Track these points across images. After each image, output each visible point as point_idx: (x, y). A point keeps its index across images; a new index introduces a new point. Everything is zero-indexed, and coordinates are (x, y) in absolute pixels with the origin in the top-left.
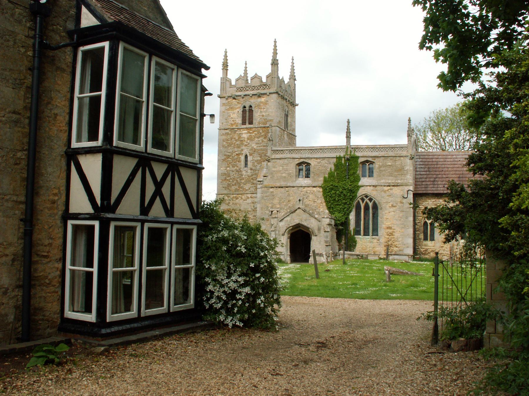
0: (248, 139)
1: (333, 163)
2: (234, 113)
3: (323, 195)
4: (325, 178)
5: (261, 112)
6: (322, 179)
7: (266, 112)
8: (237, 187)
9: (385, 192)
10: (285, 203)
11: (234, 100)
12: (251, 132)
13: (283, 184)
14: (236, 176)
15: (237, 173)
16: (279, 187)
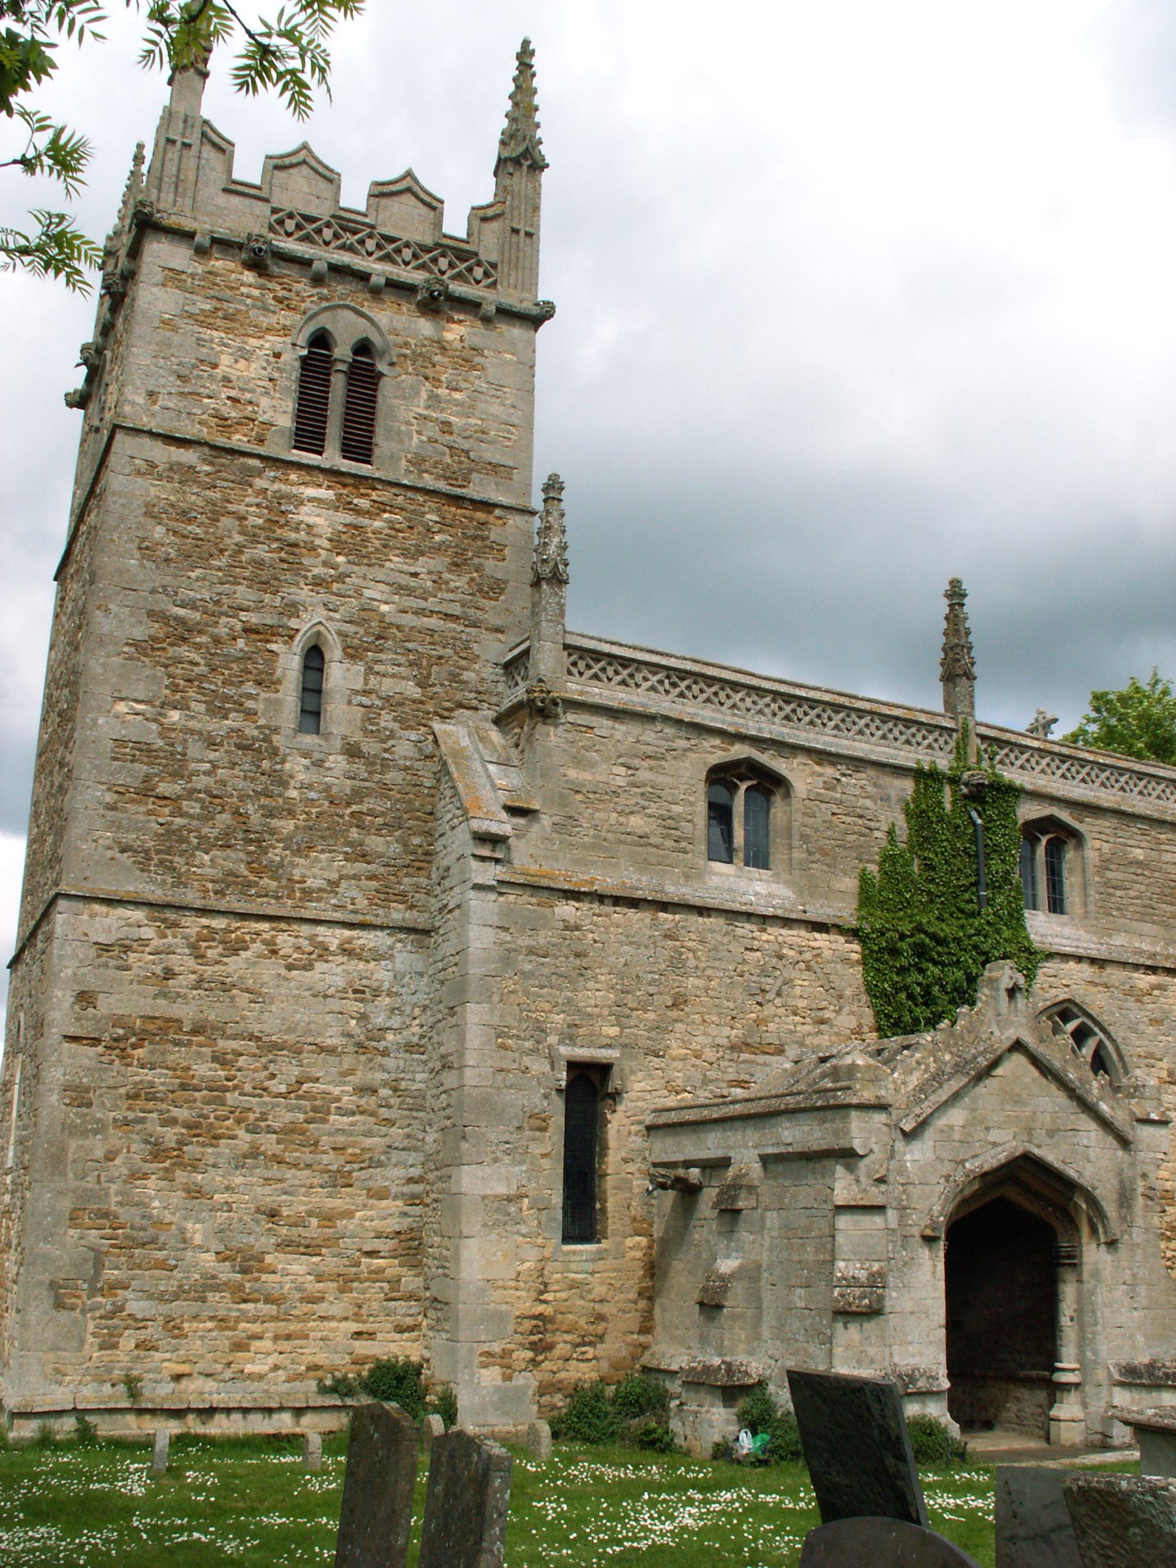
0: (338, 544)
1: (901, 799)
2: (245, 355)
3: (870, 990)
4: (864, 881)
5: (434, 400)
6: (850, 884)
7: (468, 409)
8: (235, 860)
9: (1139, 996)
10: (651, 1016)
11: (249, 277)
12: (364, 503)
13: (640, 883)
14: (236, 780)
15: (246, 760)
16: (617, 901)
